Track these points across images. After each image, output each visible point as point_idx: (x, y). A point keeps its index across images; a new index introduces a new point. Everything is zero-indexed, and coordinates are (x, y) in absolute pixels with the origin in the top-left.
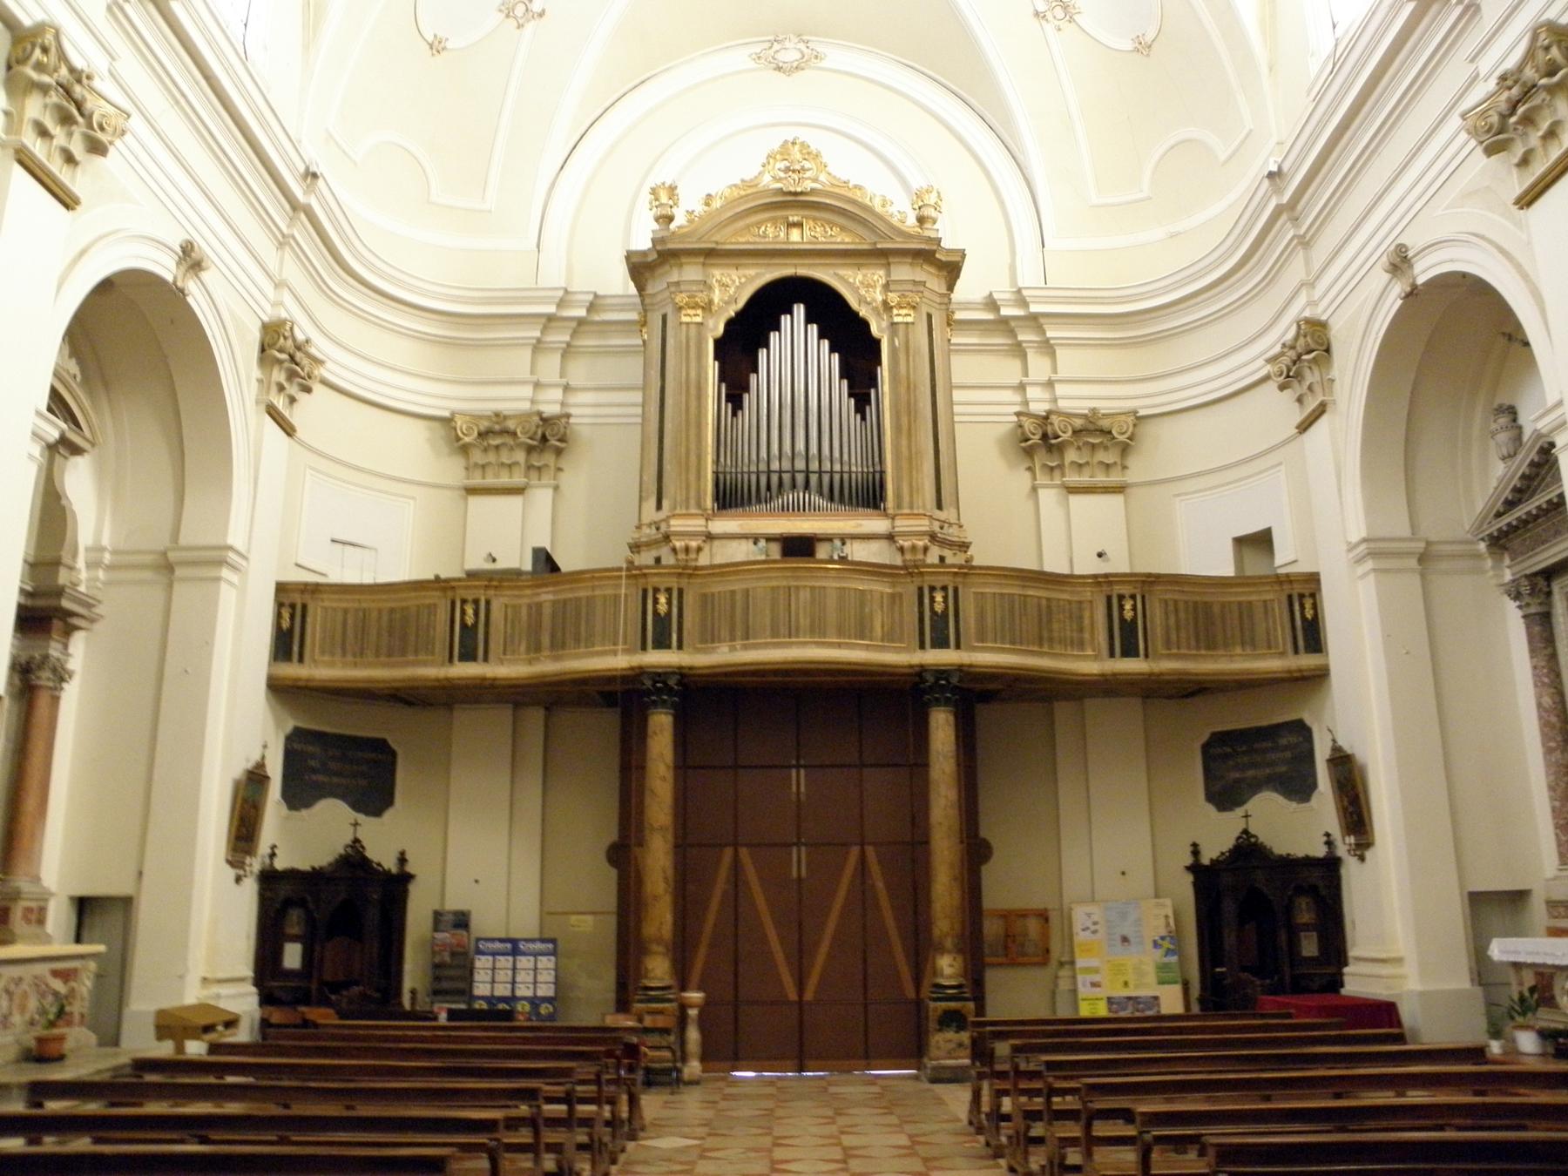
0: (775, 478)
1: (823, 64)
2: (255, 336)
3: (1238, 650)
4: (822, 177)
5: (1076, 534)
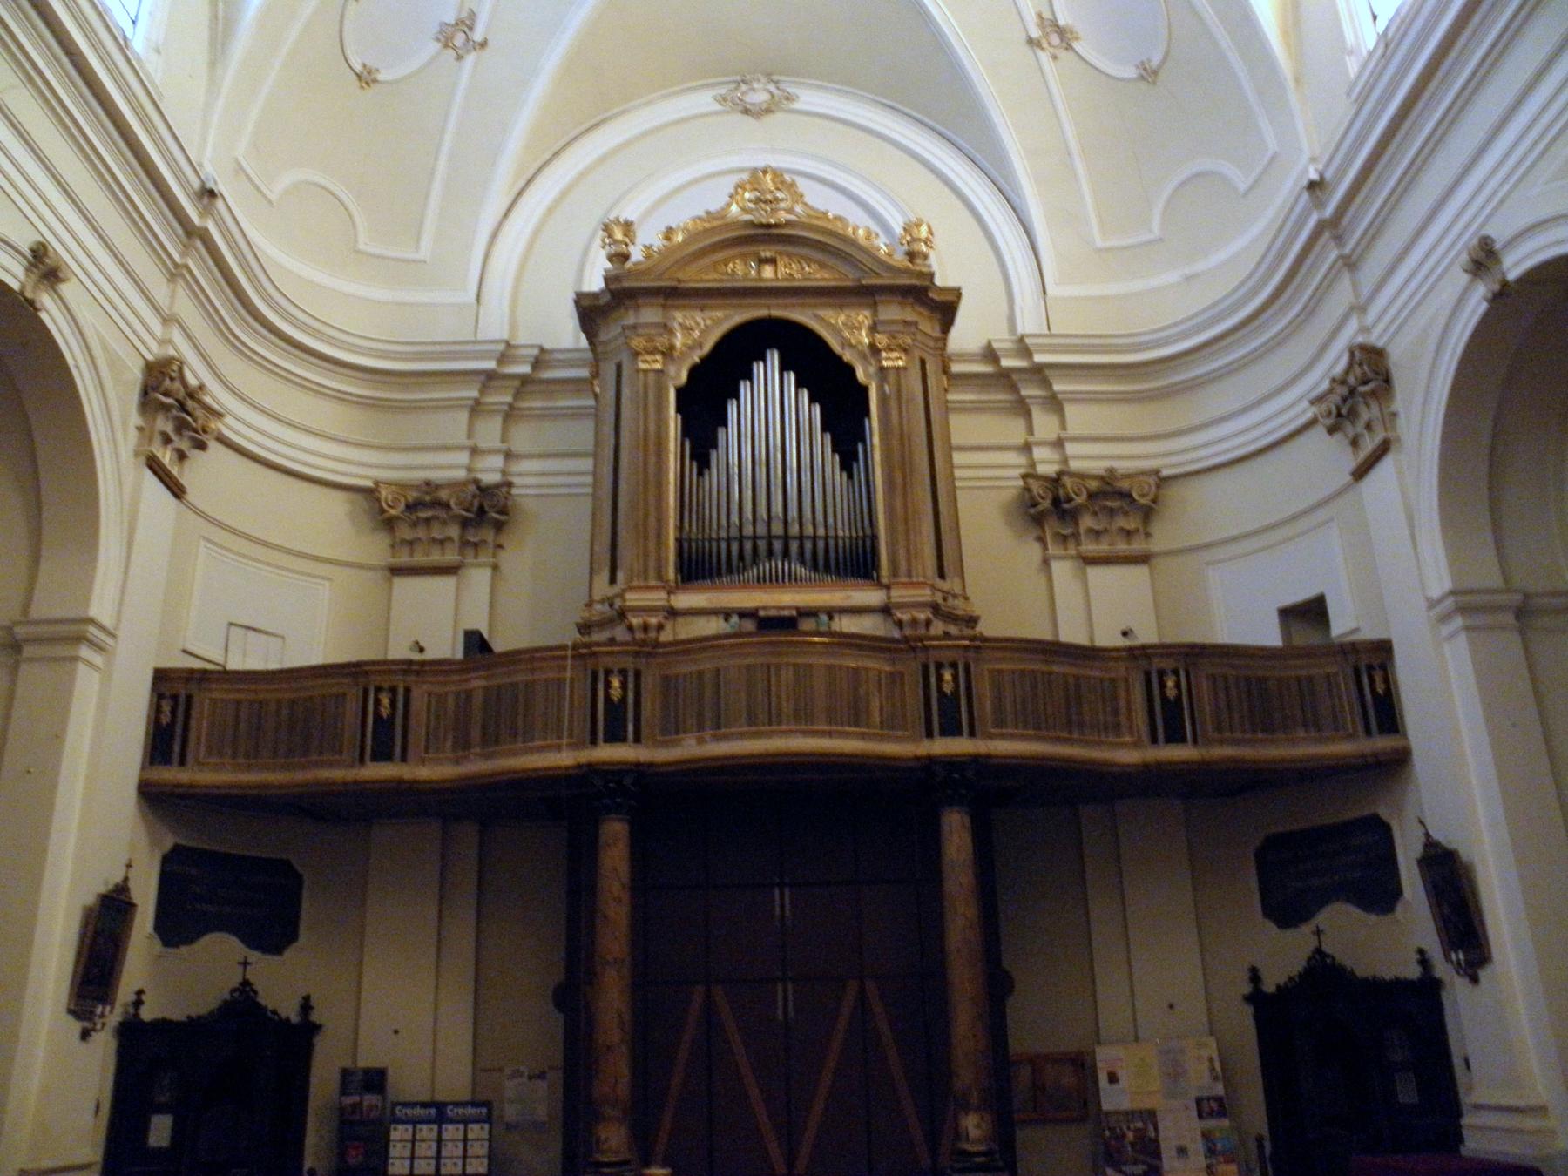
0: (748, 546)
1: (796, 106)
2: (136, 373)
3: (1302, 734)
4: (798, 209)
5: (1101, 606)
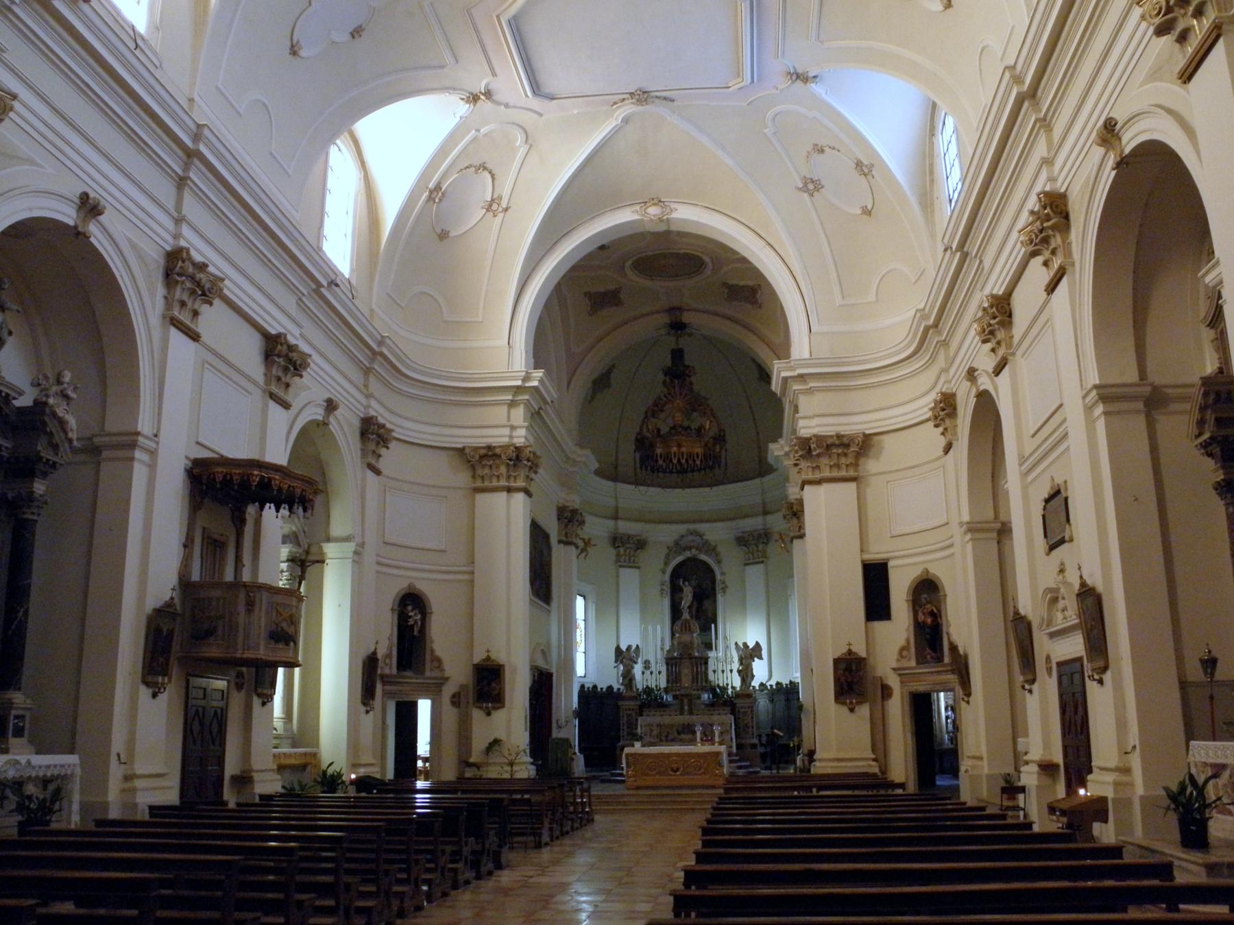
2: (357, 423)
